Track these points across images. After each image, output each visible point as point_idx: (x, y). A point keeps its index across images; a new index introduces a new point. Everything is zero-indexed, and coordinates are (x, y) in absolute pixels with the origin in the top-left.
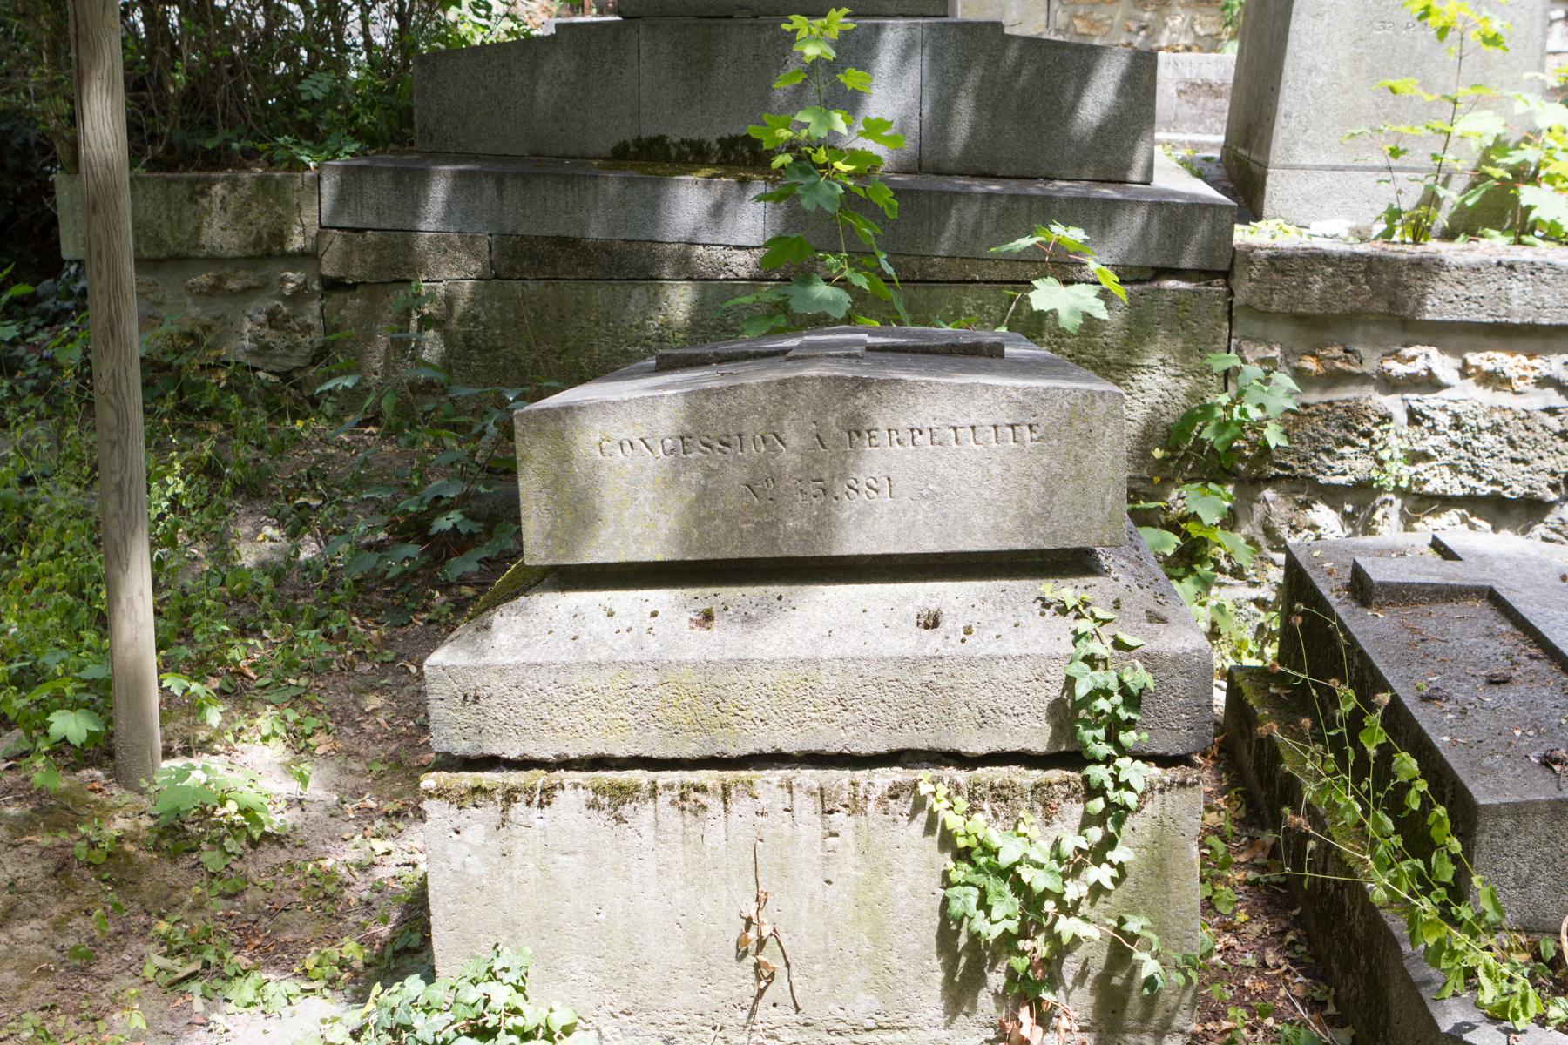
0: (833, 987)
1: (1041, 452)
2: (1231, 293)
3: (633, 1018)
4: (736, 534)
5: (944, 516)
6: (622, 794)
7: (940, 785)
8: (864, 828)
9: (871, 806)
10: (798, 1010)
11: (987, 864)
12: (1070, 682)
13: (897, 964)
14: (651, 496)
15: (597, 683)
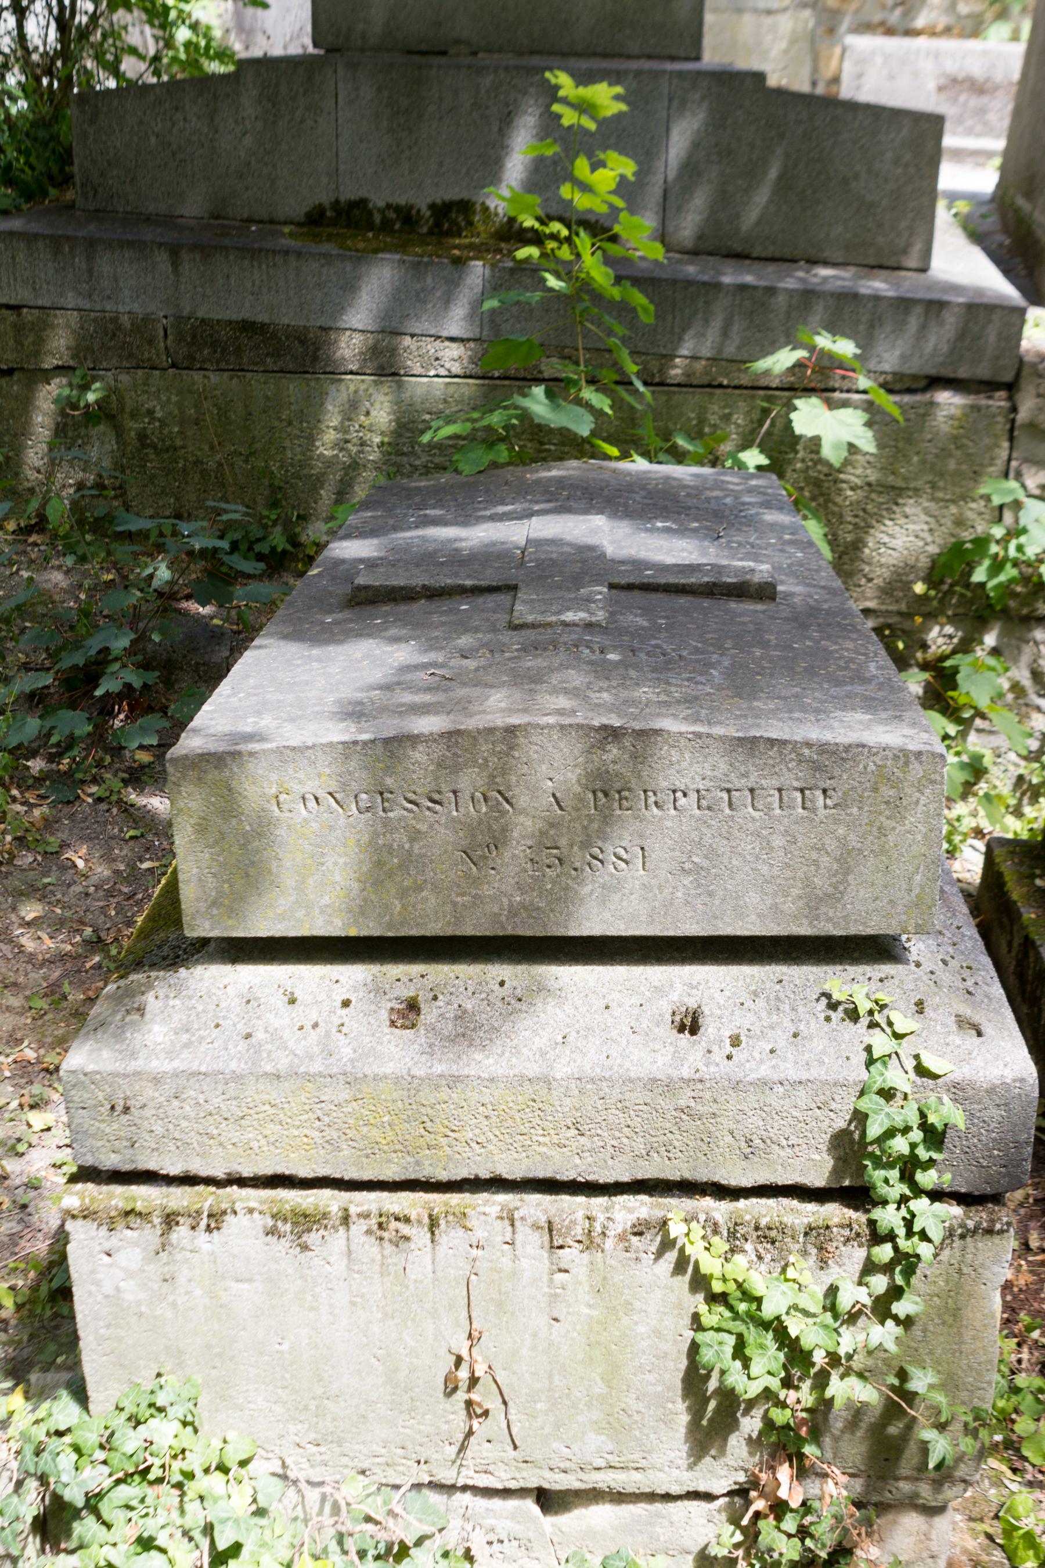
0: (557, 1426)
1: (837, 821)
2: (1014, 409)
3: (322, 1449)
4: (448, 908)
5: (711, 894)
6: (305, 1222)
7: (694, 1225)
8: (601, 1265)
9: (609, 1244)
10: (515, 1447)
11: (748, 1313)
12: (860, 1117)
13: (631, 1402)
14: (341, 861)
15: (274, 1096)
